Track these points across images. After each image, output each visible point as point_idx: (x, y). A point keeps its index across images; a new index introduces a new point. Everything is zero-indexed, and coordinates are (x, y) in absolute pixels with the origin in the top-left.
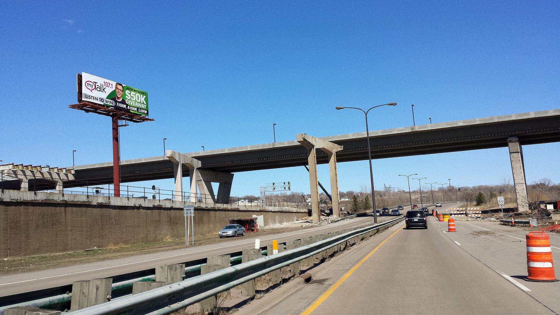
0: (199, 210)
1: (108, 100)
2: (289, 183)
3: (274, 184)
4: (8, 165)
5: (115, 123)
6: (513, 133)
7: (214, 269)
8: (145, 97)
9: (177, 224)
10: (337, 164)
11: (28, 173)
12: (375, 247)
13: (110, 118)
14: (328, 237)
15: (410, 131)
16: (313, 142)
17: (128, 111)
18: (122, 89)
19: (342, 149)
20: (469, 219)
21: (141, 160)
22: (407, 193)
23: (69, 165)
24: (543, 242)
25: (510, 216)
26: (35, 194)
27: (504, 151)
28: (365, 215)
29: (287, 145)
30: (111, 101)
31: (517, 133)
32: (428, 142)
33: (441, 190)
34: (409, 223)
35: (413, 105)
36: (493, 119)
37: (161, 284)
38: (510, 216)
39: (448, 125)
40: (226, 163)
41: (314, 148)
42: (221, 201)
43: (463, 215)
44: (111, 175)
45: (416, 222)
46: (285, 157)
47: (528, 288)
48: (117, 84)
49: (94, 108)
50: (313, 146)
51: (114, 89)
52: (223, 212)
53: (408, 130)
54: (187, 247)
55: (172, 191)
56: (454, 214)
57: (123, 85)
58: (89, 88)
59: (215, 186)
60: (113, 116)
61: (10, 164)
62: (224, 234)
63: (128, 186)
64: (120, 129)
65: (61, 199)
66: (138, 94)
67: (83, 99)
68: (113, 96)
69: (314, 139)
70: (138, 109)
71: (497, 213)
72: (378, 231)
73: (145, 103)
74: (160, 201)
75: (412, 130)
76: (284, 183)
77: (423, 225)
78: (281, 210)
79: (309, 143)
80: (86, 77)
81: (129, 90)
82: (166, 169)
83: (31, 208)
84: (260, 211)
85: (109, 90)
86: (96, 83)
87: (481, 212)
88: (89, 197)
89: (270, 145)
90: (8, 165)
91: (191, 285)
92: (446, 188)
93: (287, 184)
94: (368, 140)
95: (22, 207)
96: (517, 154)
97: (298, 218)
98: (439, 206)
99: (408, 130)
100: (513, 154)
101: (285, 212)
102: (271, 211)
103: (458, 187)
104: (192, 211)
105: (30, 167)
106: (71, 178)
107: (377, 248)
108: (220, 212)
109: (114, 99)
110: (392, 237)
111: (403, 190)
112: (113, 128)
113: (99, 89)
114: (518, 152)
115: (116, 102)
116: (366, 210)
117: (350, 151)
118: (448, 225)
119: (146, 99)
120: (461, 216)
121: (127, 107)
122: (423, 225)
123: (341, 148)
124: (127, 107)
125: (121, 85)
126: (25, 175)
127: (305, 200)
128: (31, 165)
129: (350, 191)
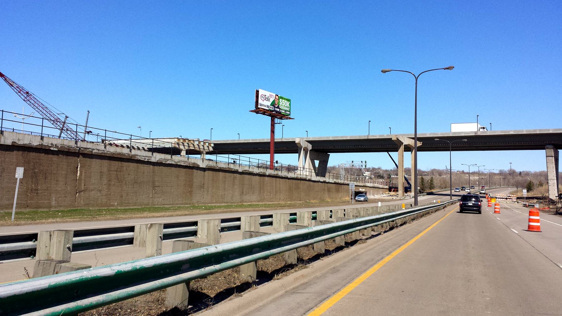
0: (271, 177)
1: (271, 106)
2: (366, 162)
3: (353, 162)
4: (174, 138)
5: (273, 121)
6: (550, 142)
7: (188, 246)
8: (289, 102)
9: (198, 185)
11: (186, 144)
12: (453, 210)
14: (429, 205)
17: (280, 113)
18: (278, 99)
19: (421, 144)
20: (508, 202)
21: (264, 140)
22: (467, 173)
24: (498, 205)
25: (541, 203)
27: (542, 153)
28: (431, 194)
29: (378, 138)
30: (272, 107)
31: (552, 142)
33: (501, 173)
35: (478, 116)
37: (201, 245)
38: (541, 203)
40: (329, 147)
41: (403, 145)
42: (320, 174)
43: (504, 199)
44: (239, 149)
46: (375, 146)
47: (517, 231)
48: (276, 95)
49: (264, 112)
51: (274, 98)
53: (473, 134)
54: (353, 204)
55: (106, 130)
56: (498, 198)
57: (279, 96)
58: (262, 99)
59: (317, 163)
61: (175, 138)
62: (359, 200)
63: (77, 125)
64: (276, 126)
66: (286, 101)
67: (259, 107)
68: (273, 104)
69: (403, 138)
70: (285, 111)
71: (533, 200)
72: (452, 204)
73: (289, 107)
74: (216, 163)
75: (475, 134)
76: (362, 162)
78: (373, 186)
80: (261, 92)
81: (282, 99)
82: (282, 148)
83: (228, 174)
84: (364, 186)
85: (272, 100)
86: (266, 95)
87: (516, 198)
88: (45, 139)
89: (365, 136)
90: (174, 138)
91: (199, 256)
92: (507, 171)
93: (364, 162)
96: (551, 157)
97: (383, 193)
98: (483, 193)
99: (473, 134)
100: (548, 157)
101: (376, 188)
102: (369, 187)
103: (520, 171)
104: (354, 186)
105: (187, 140)
106: (211, 149)
107: (376, 267)
109: (274, 106)
110: (447, 216)
111: (462, 170)
112: (271, 125)
113: (267, 100)
114: (553, 156)
115: (275, 107)
116: (431, 189)
117: (426, 145)
119: (290, 104)
121: (280, 110)
123: (421, 144)
124: (280, 110)
125: (278, 96)
126: (184, 146)
127: (362, 174)
128: (188, 139)
129: (407, 167)
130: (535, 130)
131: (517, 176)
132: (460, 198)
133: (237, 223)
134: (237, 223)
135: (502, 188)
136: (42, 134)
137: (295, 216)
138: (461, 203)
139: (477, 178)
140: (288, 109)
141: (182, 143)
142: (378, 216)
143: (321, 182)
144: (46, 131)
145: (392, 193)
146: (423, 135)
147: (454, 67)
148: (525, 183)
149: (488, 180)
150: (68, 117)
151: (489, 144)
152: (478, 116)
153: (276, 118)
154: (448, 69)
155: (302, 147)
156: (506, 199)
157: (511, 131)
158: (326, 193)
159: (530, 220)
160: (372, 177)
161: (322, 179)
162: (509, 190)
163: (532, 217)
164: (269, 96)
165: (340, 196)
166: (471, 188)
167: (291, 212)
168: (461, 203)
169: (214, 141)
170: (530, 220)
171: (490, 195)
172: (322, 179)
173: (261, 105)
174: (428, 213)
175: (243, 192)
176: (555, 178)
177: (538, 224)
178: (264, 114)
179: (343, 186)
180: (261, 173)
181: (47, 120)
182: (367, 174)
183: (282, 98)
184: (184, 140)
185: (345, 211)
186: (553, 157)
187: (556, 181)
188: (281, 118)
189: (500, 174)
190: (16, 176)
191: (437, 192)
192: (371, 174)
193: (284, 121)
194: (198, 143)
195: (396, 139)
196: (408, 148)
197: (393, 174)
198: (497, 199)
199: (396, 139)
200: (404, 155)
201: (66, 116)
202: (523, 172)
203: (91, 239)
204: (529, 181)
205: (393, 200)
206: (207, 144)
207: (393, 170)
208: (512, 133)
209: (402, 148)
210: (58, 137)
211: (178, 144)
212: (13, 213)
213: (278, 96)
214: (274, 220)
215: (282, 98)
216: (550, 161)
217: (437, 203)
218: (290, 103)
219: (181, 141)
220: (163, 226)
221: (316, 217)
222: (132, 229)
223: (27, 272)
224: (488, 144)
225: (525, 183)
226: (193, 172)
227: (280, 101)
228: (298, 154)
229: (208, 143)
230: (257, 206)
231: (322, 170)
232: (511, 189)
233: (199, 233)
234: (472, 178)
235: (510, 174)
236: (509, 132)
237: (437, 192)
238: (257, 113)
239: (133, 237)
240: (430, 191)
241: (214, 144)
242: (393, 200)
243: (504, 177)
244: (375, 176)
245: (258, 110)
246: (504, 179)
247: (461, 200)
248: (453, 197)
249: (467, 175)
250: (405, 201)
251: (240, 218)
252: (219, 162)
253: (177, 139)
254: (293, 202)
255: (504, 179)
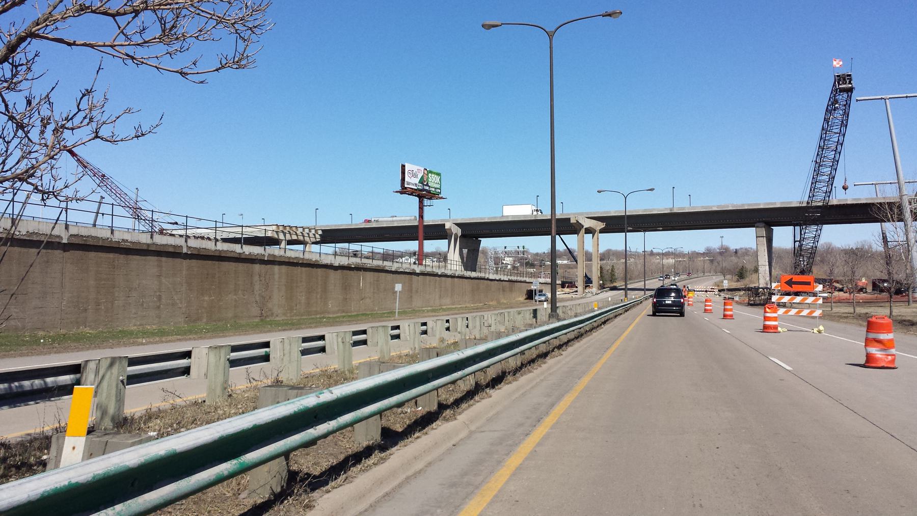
3: (505, 248)
6: (761, 220)
10: (585, 235)
11: (311, 235)
13: (417, 199)
15: (669, 212)
16: (583, 223)
17: (429, 192)
19: (604, 226)
23: (311, 224)
31: (764, 219)
32: (685, 223)
34: (658, 306)
35: (673, 188)
39: (704, 209)
43: (703, 292)
45: (669, 305)
48: (425, 169)
49: (412, 192)
52: (519, 283)
55: (216, 221)
56: (703, 291)
57: (428, 170)
59: (465, 251)
60: (418, 196)
61: (273, 225)
66: (436, 176)
72: (646, 299)
75: (670, 211)
76: (518, 247)
77: (678, 310)
80: (408, 167)
85: (420, 176)
92: (716, 249)
94: (626, 218)
105: (288, 228)
109: (422, 183)
111: (651, 250)
112: (419, 208)
115: (424, 185)
119: (440, 180)
120: (786, 312)
122: (678, 310)
131: (731, 256)
132: (653, 293)
133: (182, 363)
134: (182, 363)
135: (706, 276)
136: (66, 221)
137: (267, 350)
138: (655, 300)
139: (671, 261)
140: (438, 186)
141: (301, 233)
143: (497, 280)
144: (118, 223)
145: (567, 290)
150: (104, 198)
152: (673, 188)
153: (426, 198)
154: (610, 15)
155: (453, 233)
156: (706, 291)
157: (714, 206)
161: (474, 274)
162: (713, 279)
164: (417, 171)
168: (655, 300)
169: (321, 226)
170: (706, 306)
171: (688, 287)
172: (474, 274)
173: (408, 184)
174: (634, 306)
176: (767, 263)
177: (711, 308)
178: (411, 194)
179: (516, 283)
182: (508, 260)
183: (431, 172)
184: (284, 227)
185: (467, 320)
186: (765, 238)
187: (767, 267)
188: (430, 199)
191: (621, 286)
192: (514, 261)
194: (302, 231)
195: (575, 222)
196: (589, 231)
197: (547, 259)
198: (696, 292)
200: (585, 241)
201: (101, 197)
202: (741, 249)
205: (572, 299)
206: (313, 231)
207: (547, 253)
208: (715, 209)
209: (583, 231)
211: (277, 232)
213: (426, 170)
215: (431, 172)
216: (761, 243)
218: (440, 178)
219: (281, 228)
222: (322, 338)
223: (252, 380)
225: (737, 268)
226: (412, 277)
229: (308, 229)
230: (451, 309)
232: (716, 278)
233: (193, 371)
234: (665, 261)
235: (721, 253)
236: (711, 208)
238: (401, 193)
240: (612, 285)
241: (323, 231)
242: (572, 299)
243: (712, 258)
244: (522, 265)
245: (404, 190)
246: (712, 261)
247: (655, 296)
249: (658, 257)
250: (587, 299)
251: (269, 342)
252: (29, 219)
253: (276, 226)
255: (712, 261)
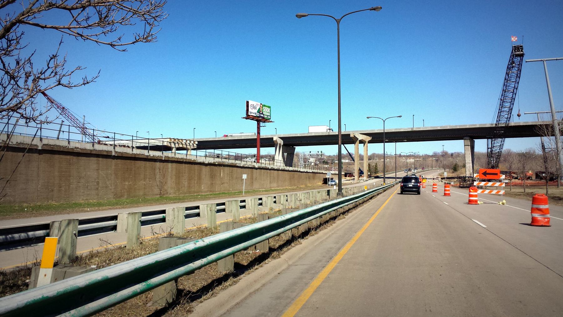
3: (310, 152)
4: (166, 138)
11: (191, 144)
15: (411, 130)
16: (358, 137)
17: (263, 118)
23: (191, 138)
26: (148, 152)
31: (469, 135)
32: (420, 137)
35: (413, 115)
36: (457, 127)
39: (432, 128)
43: (432, 180)
48: (261, 104)
49: (253, 118)
50: (358, 139)
52: (319, 174)
55: (133, 136)
56: (432, 179)
57: (263, 104)
60: (257, 120)
61: (168, 138)
65: (91, 148)
66: (267, 108)
67: (249, 114)
68: (259, 111)
72: (397, 184)
76: (318, 152)
77: (417, 190)
79: (356, 138)
80: (251, 103)
85: (258, 108)
90: (166, 138)
94: (384, 134)
95: (94, 159)
104: (331, 174)
105: (176, 140)
108: (237, 168)
109: (259, 113)
111: (399, 154)
112: (257, 128)
115: (260, 113)
118: (445, 190)
122: (417, 190)
125: (262, 104)
130: (456, 126)
131: (449, 157)
132: (401, 180)
133: (196, 211)
134: (196, 211)
136: (41, 136)
137: (164, 215)
138: (402, 184)
139: (412, 160)
140: (269, 114)
141: (185, 143)
142: (377, 189)
145: (348, 178)
146: (372, 131)
147: (381, 8)
148: (452, 165)
149: (422, 163)
150: (64, 122)
151: (422, 137)
152: (413, 115)
153: (262, 122)
155: (278, 143)
157: (438, 127)
158: (308, 180)
159: (433, 188)
160: (317, 163)
161: (291, 169)
163: (434, 186)
164: (256, 105)
165: (315, 181)
166: (409, 171)
167: (143, 211)
170: (433, 188)
171: (422, 177)
172: (291, 169)
173: (251, 113)
175: (271, 182)
178: (253, 119)
179: (317, 174)
180: (278, 169)
181: (75, 127)
182: (312, 160)
184: (175, 139)
185: (287, 197)
187: (471, 164)
188: (264, 122)
189: (434, 156)
190: (243, 178)
192: (316, 160)
193: (267, 124)
195: (353, 136)
196: (362, 142)
198: (427, 179)
199: (353, 136)
200: (359, 148)
201: (62, 121)
203: (84, 227)
204: (455, 164)
205: (351, 184)
207: (336, 156)
209: (358, 142)
210: (56, 139)
212: (244, 191)
213: (262, 104)
214: (118, 222)
215: (265, 106)
217: (390, 183)
218: (270, 109)
219: (173, 140)
220: (216, 205)
221: (262, 203)
224: (421, 137)
225: (452, 165)
227: (264, 109)
228: (275, 148)
231: (289, 161)
232: (439, 171)
233: (118, 228)
234: (408, 161)
235: (443, 156)
236: (437, 128)
237: (381, 176)
238: (247, 118)
239: (116, 224)
240: (376, 175)
241: (198, 142)
242: (351, 184)
244: (320, 163)
245: (248, 117)
246: (437, 160)
247: (402, 182)
248: (397, 180)
251: (165, 210)
253: (169, 139)
254: (292, 187)
255: (437, 160)
